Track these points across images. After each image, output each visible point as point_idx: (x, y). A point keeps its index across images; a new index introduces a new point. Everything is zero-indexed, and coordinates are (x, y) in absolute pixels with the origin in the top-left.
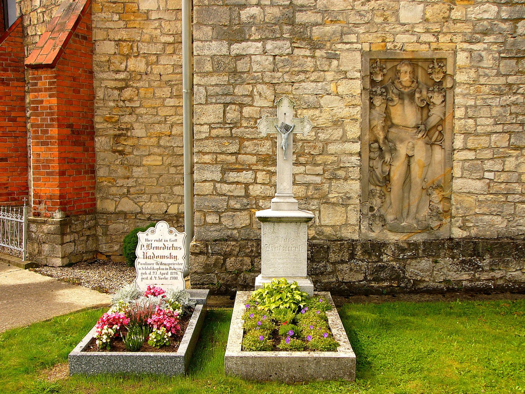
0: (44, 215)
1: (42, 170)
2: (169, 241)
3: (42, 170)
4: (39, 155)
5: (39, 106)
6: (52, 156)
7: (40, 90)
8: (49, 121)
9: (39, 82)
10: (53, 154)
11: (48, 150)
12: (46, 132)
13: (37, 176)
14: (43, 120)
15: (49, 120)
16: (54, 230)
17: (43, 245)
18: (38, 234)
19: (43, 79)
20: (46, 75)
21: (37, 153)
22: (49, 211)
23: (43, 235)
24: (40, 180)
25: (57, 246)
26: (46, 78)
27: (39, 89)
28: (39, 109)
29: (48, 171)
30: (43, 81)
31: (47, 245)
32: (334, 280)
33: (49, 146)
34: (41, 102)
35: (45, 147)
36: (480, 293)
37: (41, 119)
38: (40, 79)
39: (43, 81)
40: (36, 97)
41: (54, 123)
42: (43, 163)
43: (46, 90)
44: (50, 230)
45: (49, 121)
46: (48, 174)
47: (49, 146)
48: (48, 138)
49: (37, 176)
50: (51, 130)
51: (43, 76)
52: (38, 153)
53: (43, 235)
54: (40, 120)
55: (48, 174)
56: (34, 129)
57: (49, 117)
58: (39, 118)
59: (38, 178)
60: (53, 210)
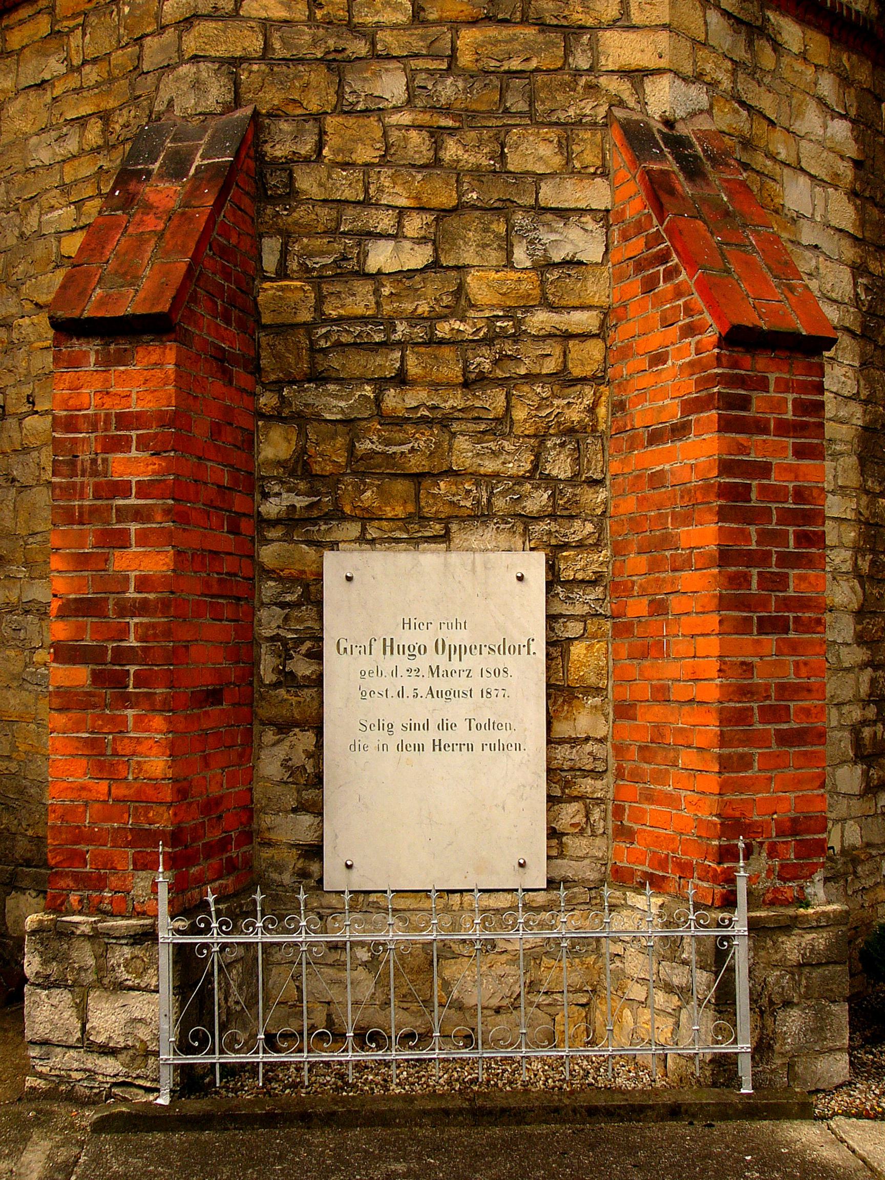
0: (770, 896)
1: (761, 727)
2: (477, 747)
3: (761, 727)
4: (748, 668)
5: (755, 483)
6: (804, 671)
7: (760, 427)
8: (791, 543)
9: (755, 394)
10: (805, 664)
11: (786, 651)
12: (781, 581)
13: (740, 750)
14: (765, 536)
15: (791, 538)
16: (828, 948)
17: (780, 1015)
18: (765, 973)
19: (772, 389)
20: (787, 376)
21: (743, 663)
22: (785, 880)
23: (782, 976)
24: (749, 766)
25: (834, 1008)
26: (784, 386)
27: (757, 421)
28: (753, 496)
29: (785, 726)
30: (772, 394)
31: (795, 1012)
32: (32, 339)
33: (792, 635)
34: (764, 470)
35: (776, 637)
36: (768, 41)
37: (762, 534)
38: (762, 384)
39: (772, 394)
40: (742, 449)
41: (813, 550)
42: (768, 697)
43: (784, 428)
44: (812, 951)
45: (791, 543)
46: (784, 738)
47: (792, 635)
48: (786, 604)
49: (740, 750)
50: (802, 578)
51: (772, 377)
52: (749, 660)
53: (782, 976)
54: (754, 538)
55: (784, 738)
56: (734, 569)
57: (791, 529)
58: (752, 529)
59: (742, 756)
60: (806, 872)
